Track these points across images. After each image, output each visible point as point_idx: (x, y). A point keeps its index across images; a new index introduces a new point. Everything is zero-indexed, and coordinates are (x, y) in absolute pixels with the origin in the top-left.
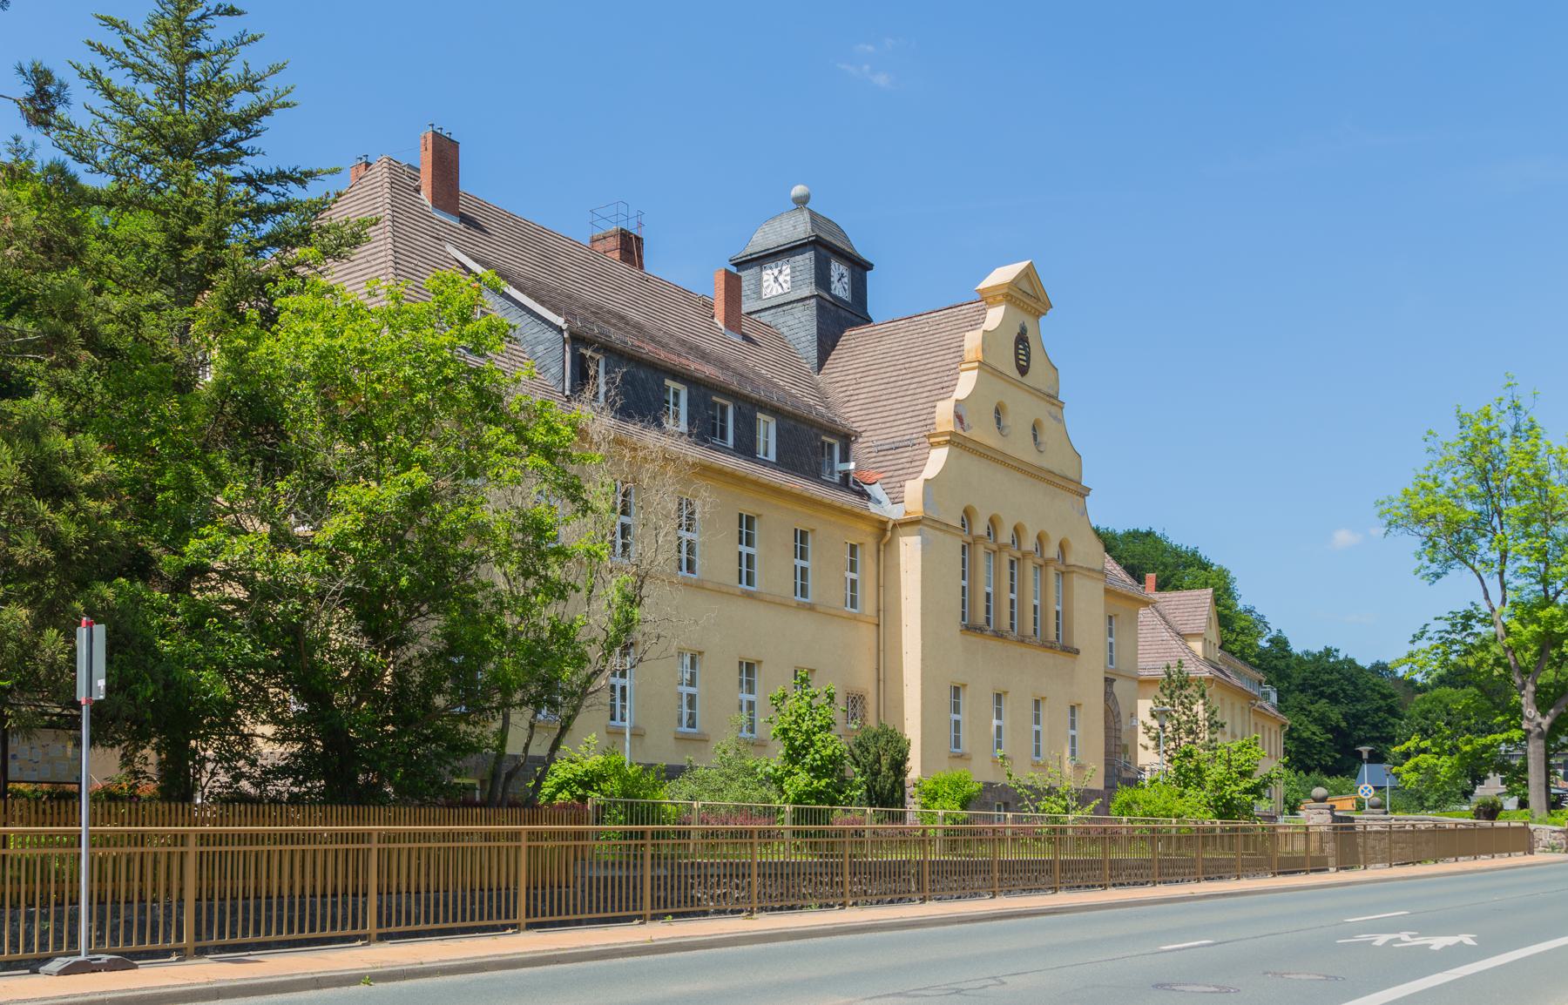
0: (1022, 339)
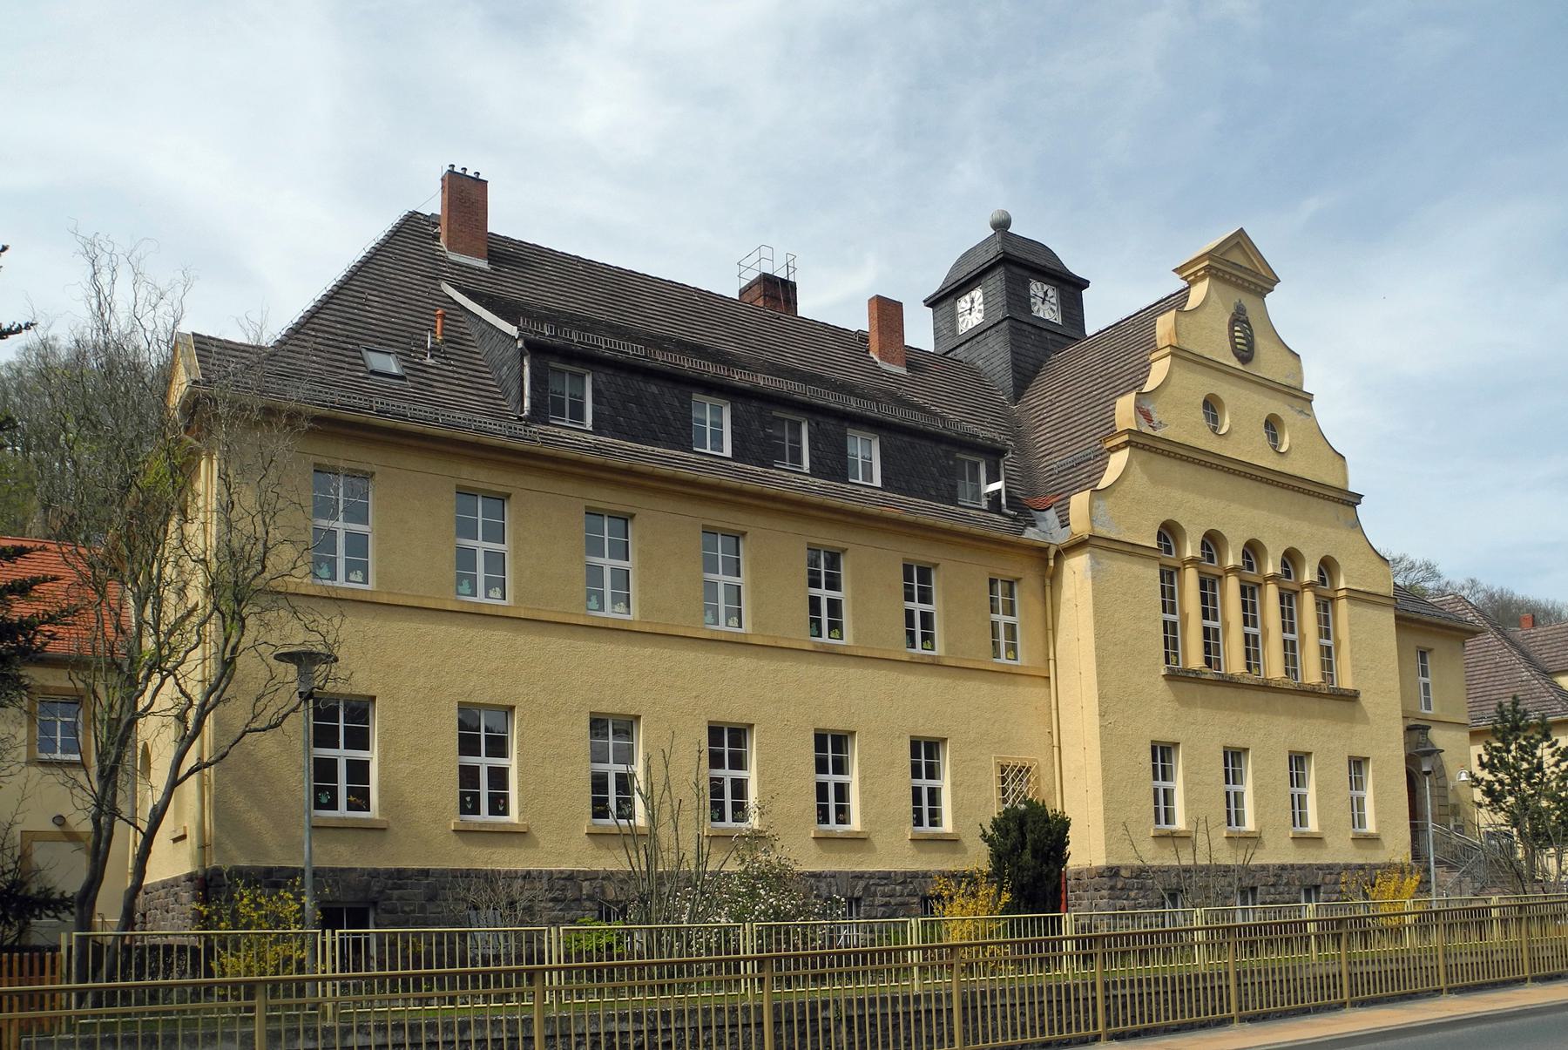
0: (1239, 318)
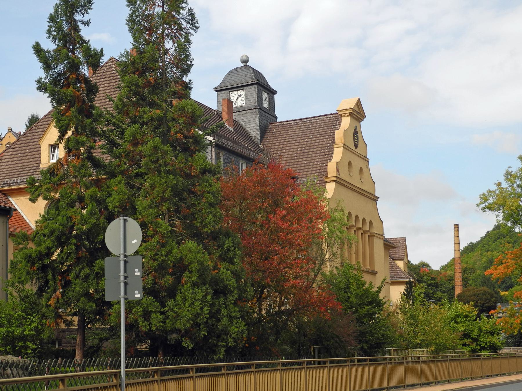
0: (356, 133)
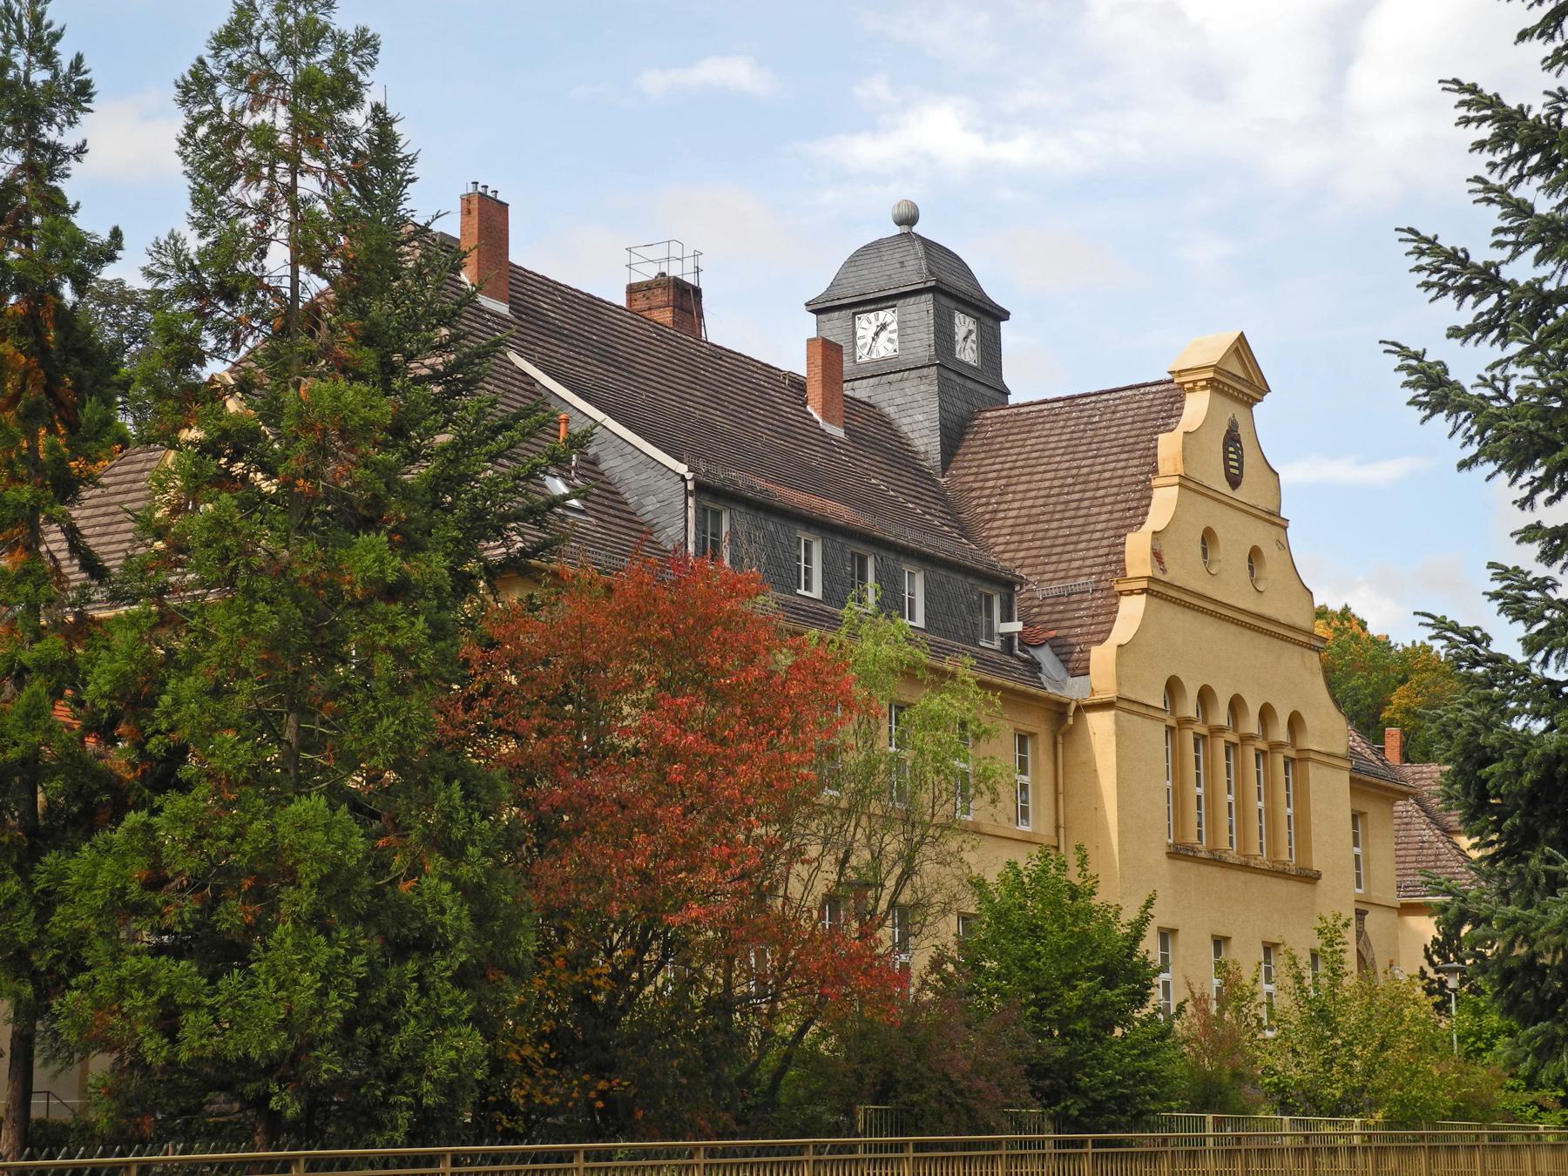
0: (1232, 438)
